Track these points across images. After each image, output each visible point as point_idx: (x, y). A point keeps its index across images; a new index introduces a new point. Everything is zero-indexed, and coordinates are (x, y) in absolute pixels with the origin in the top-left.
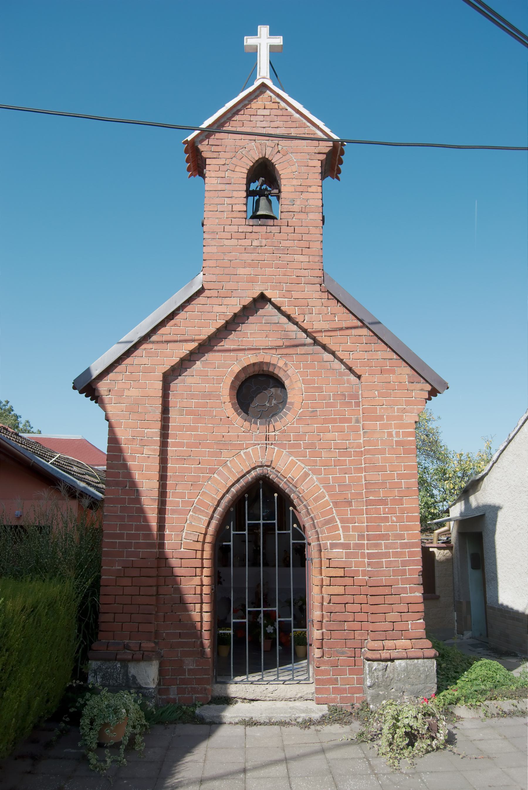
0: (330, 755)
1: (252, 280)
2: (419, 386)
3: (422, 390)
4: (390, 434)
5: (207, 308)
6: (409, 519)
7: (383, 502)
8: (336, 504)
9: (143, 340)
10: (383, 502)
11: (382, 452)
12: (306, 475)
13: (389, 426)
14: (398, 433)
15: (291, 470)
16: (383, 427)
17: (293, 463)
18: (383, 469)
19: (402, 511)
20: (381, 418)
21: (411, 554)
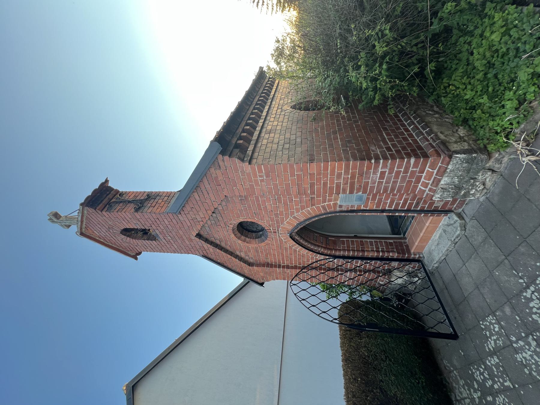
0: (445, 291)
1: (191, 240)
2: (221, 163)
3: (223, 161)
4: (262, 181)
5: (213, 254)
6: (326, 169)
7: (312, 185)
8: (312, 205)
9: (203, 237)
10: (312, 185)
11: (276, 186)
12: (295, 218)
13: (256, 182)
14: (260, 176)
15: (290, 223)
16: (257, 184)
17: (288, 223)
18: (288, 185)
19: (319, 174)
20: (252, 186)
21: (354, 167)
